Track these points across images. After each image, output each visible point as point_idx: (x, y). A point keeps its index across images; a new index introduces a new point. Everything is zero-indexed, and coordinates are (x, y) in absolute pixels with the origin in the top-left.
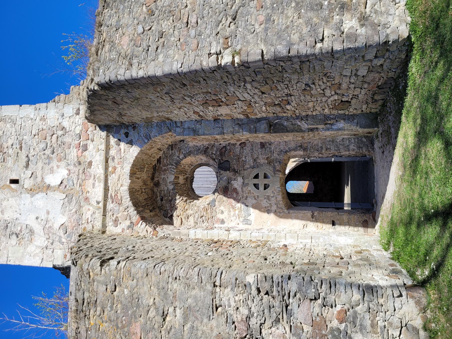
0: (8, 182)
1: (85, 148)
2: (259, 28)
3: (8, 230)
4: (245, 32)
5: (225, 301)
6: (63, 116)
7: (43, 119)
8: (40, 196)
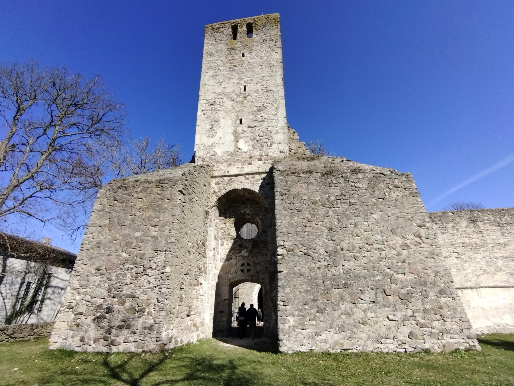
0: (240, 118)
1: (260, 160)
2: (296, 269)
3: (214, 123)
4: (295, 262)
5: (159, 256)
6: (279, 143)
7: (277, 132)
8: (232, 137)
